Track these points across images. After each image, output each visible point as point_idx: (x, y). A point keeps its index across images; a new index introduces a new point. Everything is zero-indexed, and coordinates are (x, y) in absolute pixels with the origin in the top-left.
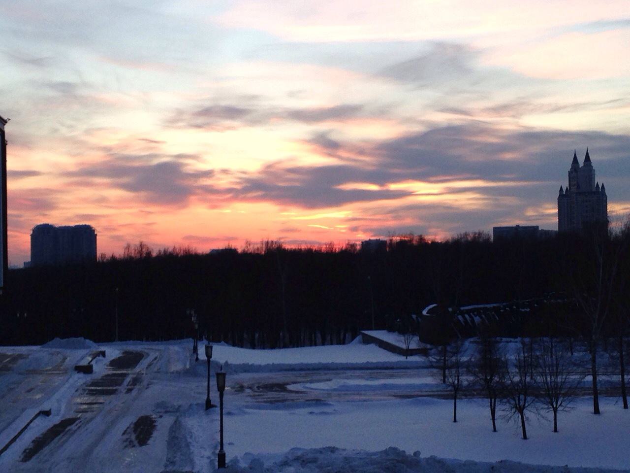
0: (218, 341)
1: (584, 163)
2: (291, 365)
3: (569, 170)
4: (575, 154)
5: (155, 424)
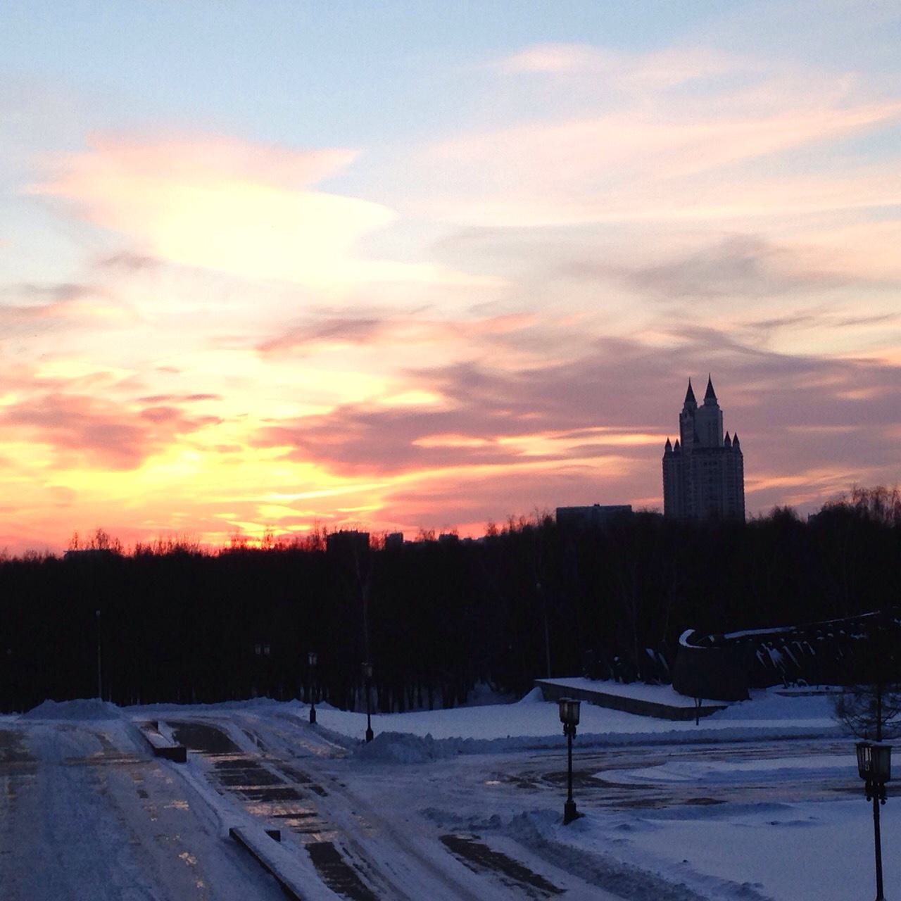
0: (705, 698)
1: (705, 400)
2: (539, 739)
3: (681, 412)
4: (690, 387)
5: (574, 847)
